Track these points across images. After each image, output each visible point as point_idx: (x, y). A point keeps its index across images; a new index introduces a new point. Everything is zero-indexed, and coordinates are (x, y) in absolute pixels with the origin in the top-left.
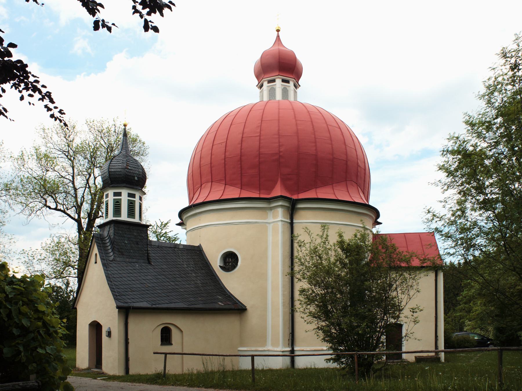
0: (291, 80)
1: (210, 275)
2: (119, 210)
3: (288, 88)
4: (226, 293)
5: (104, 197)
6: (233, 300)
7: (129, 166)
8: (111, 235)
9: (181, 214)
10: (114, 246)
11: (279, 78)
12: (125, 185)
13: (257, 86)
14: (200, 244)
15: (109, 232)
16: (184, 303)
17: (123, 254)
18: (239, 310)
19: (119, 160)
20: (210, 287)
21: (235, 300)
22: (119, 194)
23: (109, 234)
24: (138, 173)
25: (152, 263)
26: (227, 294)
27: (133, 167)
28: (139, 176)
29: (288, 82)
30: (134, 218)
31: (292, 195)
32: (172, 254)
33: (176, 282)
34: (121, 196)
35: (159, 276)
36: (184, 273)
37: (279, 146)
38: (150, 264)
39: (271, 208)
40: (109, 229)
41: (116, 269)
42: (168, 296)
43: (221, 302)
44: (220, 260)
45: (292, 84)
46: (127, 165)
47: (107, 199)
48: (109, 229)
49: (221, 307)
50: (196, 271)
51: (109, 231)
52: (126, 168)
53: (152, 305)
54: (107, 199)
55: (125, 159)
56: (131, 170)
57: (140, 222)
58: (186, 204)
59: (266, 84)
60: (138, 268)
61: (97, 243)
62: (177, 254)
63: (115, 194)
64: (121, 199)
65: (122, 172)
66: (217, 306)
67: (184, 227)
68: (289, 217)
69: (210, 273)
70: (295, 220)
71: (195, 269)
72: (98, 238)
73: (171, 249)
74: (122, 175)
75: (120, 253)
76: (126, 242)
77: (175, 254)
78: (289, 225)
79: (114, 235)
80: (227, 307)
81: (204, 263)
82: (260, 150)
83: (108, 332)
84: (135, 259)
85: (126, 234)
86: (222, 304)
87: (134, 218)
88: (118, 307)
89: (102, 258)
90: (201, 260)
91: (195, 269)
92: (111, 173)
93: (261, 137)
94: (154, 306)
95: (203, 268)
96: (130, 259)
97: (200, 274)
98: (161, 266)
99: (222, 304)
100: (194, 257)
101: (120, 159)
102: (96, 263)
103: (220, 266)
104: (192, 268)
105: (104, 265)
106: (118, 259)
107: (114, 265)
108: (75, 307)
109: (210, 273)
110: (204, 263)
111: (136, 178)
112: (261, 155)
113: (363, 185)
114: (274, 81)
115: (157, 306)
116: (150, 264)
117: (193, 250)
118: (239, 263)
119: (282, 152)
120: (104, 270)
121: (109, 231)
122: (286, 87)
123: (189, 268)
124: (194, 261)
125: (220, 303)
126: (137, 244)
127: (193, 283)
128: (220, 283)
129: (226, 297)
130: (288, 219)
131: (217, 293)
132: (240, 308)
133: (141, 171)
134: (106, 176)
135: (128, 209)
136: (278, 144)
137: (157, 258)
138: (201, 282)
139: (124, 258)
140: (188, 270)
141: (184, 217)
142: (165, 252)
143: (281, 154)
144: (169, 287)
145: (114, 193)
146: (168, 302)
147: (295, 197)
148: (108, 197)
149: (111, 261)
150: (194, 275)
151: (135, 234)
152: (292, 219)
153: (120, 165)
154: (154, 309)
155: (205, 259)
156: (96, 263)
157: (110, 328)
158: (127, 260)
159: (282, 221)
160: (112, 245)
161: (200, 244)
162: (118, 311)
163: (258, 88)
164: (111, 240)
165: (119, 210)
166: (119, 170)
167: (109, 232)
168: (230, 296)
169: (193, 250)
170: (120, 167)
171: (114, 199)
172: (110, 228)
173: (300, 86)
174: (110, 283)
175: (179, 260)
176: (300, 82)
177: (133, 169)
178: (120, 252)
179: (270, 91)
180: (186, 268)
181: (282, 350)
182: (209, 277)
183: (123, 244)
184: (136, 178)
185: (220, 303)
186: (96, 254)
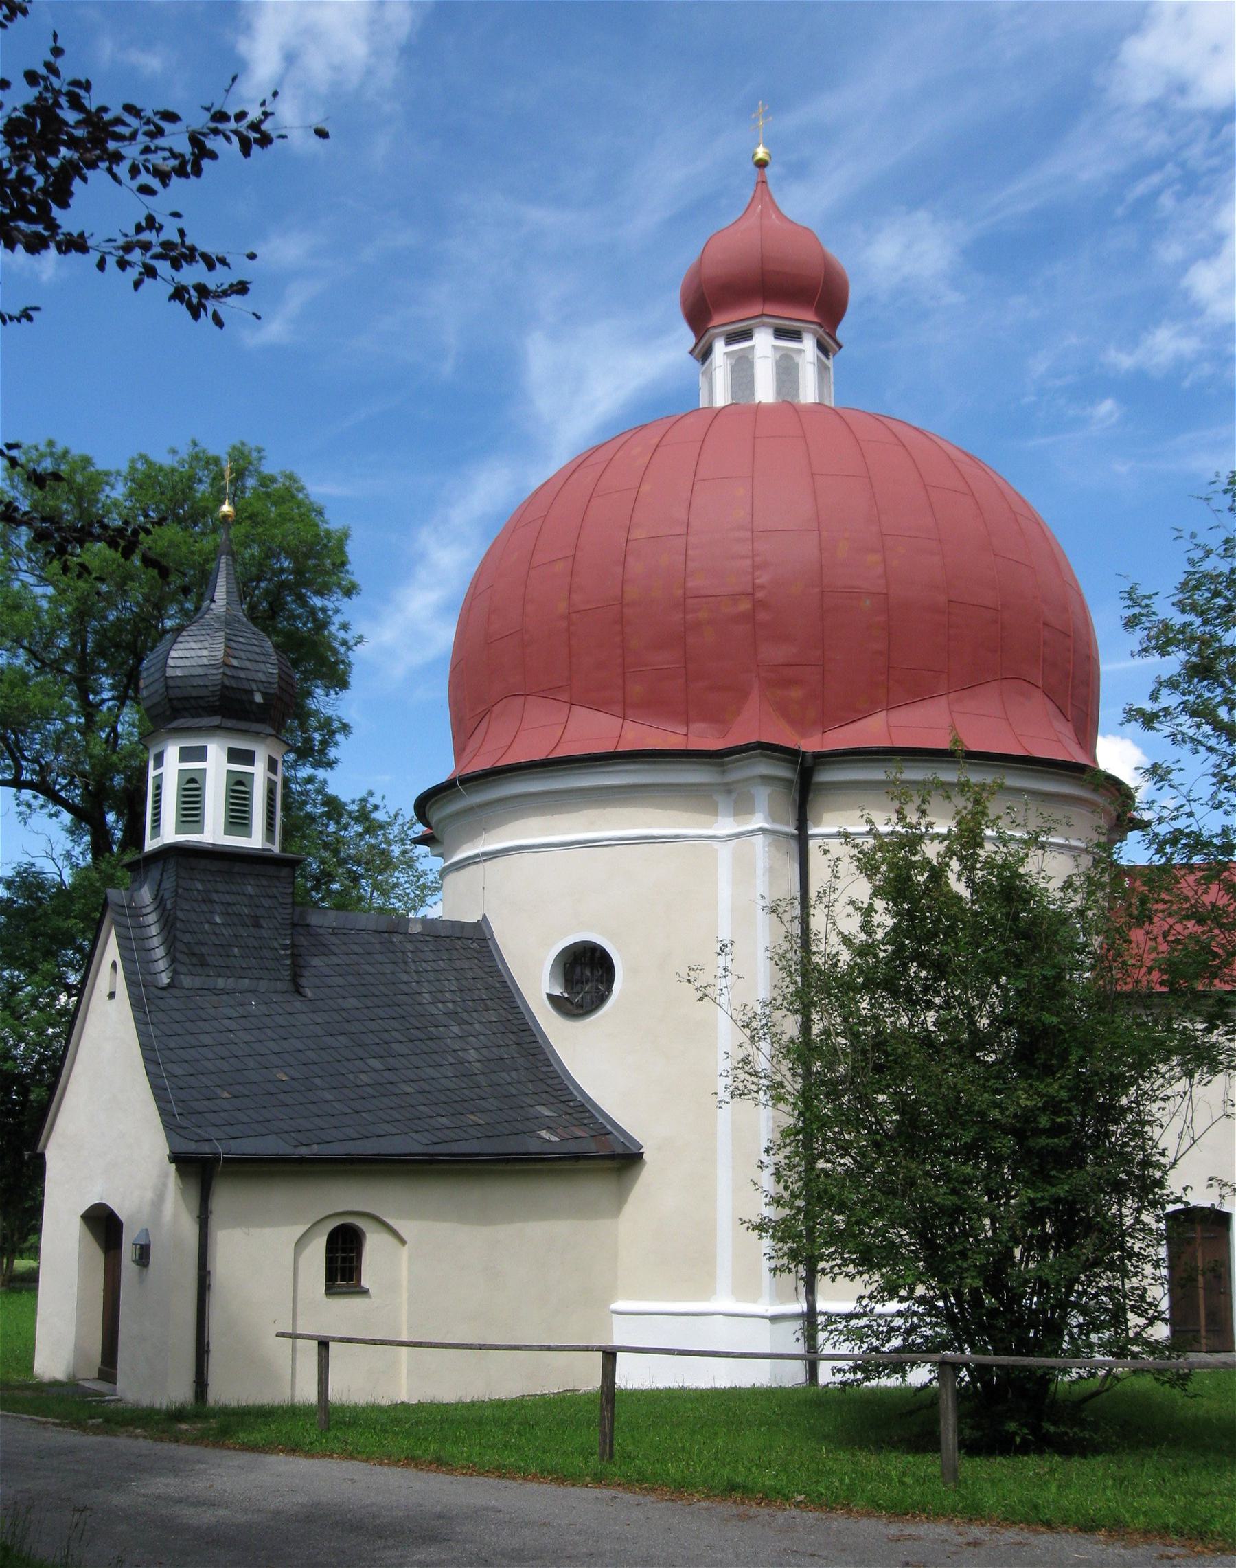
0: (809, 331)
1: (515, 1030)
2: (196, 809)
3: (796, 358)
4: (572, 1093)
5: (151, 764)
6: (596, 1122)
7: (235, 658)
8: (166, 897)
9: (424, 804)
10: (175, 937)
11: (764, 325)
12: (216, 720)
13: (691, 352)
14: (484, 917)
15: (159, 886)
16: (413, 1135)
17: (203, 964)
18: (612, 1157)
19: (201, 638)
20: (514, 1074)
21: (601, 1120)
22: (200, 754)
23: (161, 893)
24: (263, 678)
25: (309, 993)
26: (574, 1100)
27: (250, 660)
28: (268, 691)
29: (795, 335)
30: (249, 835)
31: (803, 735)
32: (379, 957)
33: (391, 1060)
34: (205, 760)
35: (329, 1040)
36: (419, 1025)
37: (754, 567)
38: (300, 993)
39: (727, 784)
40: (162, 875)
41: (177, 1016)
42: (357, 1112)
43: (549, 1129)
44: (552, 967)
45: (808, 345)
46: (227, 655)
47: (158, 772)
48: (162, 875)
49: (547, 1148)
50: (465, 1015)
51: (161, 881)
52: (225, 664)
53: (295, 1146)
54: (158, 772)
55: (222, 633)
56: (242, 669)
57: (268, 846)
58: (442, 769)
59: (720, 347)
60: (258, 1013)
61: (119, 925)
62: (399, 955)
63: (186, 755)
64: (205, 769)
65: (210, 677)
66: (533, 1146)
67: (439, 850)
68: (791, 815)
69: (516, 1022)
70: (817, 825)
71: (460, 1010)
72: (123, 907)
73: (377, 935)
74: (211, 689)
75: (194, 960)
76: (218, 920)
77: (391, 955)
78: (794, 846)
79: (177, 895)
80: (573, 1147)
81: (498, 985)
82: (689, 584)
83: (142, 1247)
84: (247, 981)
85: (217, 892)
86: (554, 1138)
87: (249, 835)
88: (175, 1158)
89: (133, 977)
90: (484, 975)
91: (460, 1010)
92: (171, 683)
93: (691, 540)
94: (304, 1151)
95: (488, 1002)
96: (231, 980)
97: (477, 1026)
98: (340, 1001)
99: (554, 1138)
100: (458, 964)
101: (204, 632)
102: (112, 995)
103: (551, 997)
104: (450, 1005)
105: (137, 1004)
106: (186, 981)
107: (172, 1002)
108: (39, 1151)
109: (516, 1022)
110: (498, 985)
111: (258, 698)
112: (689, 601)
113: (182, 1133)
114: (746, 335)
115: (315, 1149)
116: (300, 993)
117: (459, 938)
118: (617, 986)
119: (762, 587)
120: (137, 1021)
121: (161, 881)
122: (790, 353)
123: (440, 1005)
124: (457, 980)
125: (544, 1134)
126: (257, 925)
127: (452, 1060)
128: (550, 1056)
129: (570, 1111)
130: (787, 824)
131: (535, 1096)
132: (619, 1150)
133: (276, 671)
134: (157, 691)
135: (228, 803)
136: (749, 562)
137: (327, 971)
138: (481, 1058)
139: (208, 976)
140: (435, 1011)
141: (434, 817)
142: (356, 948)
143: (760, 595)
144: (362, 1076)
145: (181, 748)
146: (357, 1136)
147: (810, 744)
148: (162, 765)
149: (163, 989)
150: (456, 1029)
151: (250, 890)
152: (802, 824)
153: (205, 653)
154: (302, 1160)
155: (498, 971)
156: (112, 995)
157: (147, 1230)
158: (221, 983)
159: (762, 831)
160: (169, 933)
161: (484, 917)
162: (178, 1169)
163: (696, 358)
164: (166, 913)
165: (196, 809)
166: (200, 671)
167: (159, 886)
168: (583, 1105)
169: (459, 938)
170: (205, 662)
171: (180, 770)
172: (163, 871)
173: (840, 347)
174: (152, 1067)
175: (405, 977)
176: (842, 332)
177: (248, 664)
178: (194, 954)
179: (733, 370)
180: (430, 1008)
181: (769, 1313)
182: (511, 1036)
183: (207, 926)
184: (258, 698)
185: (544, 1134)
186: (114, 965)
